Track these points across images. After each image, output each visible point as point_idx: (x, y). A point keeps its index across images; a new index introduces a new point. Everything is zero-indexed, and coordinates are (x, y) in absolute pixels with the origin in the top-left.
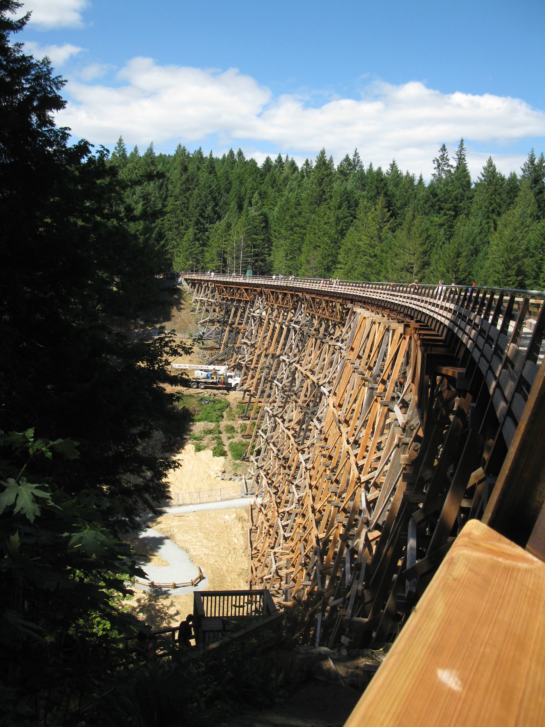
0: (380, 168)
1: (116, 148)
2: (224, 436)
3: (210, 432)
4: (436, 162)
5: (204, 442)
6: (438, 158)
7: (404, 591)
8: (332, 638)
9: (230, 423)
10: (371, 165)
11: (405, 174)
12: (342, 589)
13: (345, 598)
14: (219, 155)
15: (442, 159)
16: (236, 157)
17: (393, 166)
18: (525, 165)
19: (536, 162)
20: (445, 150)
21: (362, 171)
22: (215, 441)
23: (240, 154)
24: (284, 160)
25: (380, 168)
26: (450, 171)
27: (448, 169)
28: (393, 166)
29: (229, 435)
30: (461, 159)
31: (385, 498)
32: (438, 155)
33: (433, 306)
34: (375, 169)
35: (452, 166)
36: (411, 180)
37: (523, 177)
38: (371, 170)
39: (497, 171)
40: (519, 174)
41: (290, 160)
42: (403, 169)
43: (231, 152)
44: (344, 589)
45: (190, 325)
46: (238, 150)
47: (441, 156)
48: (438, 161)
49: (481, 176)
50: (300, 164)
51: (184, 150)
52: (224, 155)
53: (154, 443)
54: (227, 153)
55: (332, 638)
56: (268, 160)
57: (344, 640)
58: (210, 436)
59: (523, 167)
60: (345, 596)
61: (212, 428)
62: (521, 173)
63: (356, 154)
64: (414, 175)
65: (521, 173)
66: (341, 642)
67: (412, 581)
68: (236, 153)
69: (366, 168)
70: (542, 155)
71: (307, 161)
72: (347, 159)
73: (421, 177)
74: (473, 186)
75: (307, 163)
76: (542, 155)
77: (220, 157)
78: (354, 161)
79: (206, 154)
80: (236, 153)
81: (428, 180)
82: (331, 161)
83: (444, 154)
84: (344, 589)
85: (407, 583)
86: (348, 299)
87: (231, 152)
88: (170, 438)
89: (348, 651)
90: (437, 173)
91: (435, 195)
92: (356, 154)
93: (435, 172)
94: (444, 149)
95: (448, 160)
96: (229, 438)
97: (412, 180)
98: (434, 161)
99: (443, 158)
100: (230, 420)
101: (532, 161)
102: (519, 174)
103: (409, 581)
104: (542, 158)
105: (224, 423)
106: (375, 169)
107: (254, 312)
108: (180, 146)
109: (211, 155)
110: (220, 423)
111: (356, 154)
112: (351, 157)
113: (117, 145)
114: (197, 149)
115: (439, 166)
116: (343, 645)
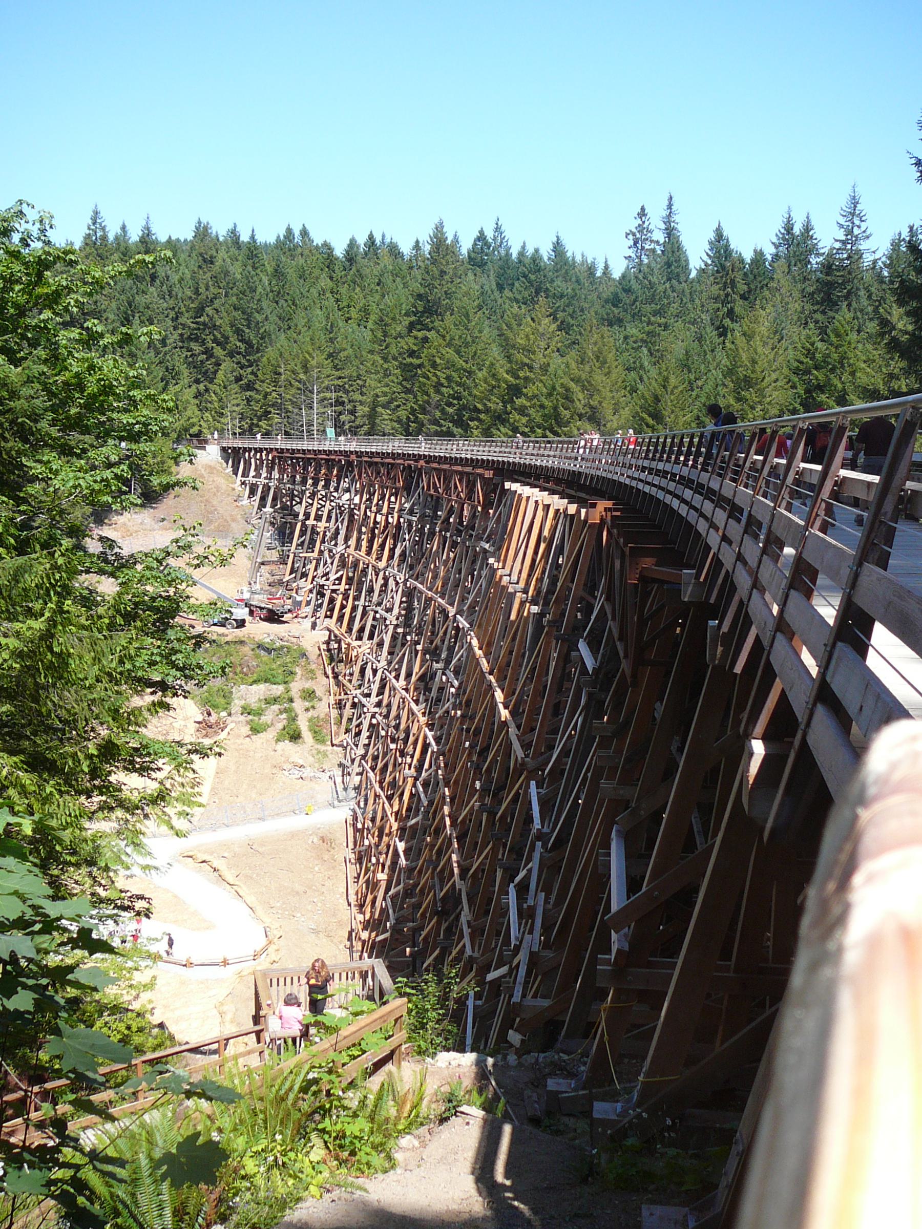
0: (537, 251)
1: (89, 229)
2: (299, 705)
3: (275, 700)
4: (631, 237)
5: (266, 718)
6: (634, 230)
7: (609, 951)
8: (493, 1035)
9: (308, 685)
10: (524, 247)
11: (578, 259)
12: (506, 951)
13: (511, 966)
14: (268, 235)
15: (640, 232)
16: (298, 238)
17: (558, 247)
18: (777, 235)
19: (797, 230)
20: (645, 215)
21: (508, 255)
22: (284, 716)
23: (304, 233)
24: (378, 242)
25: (537, 251)
26: (654, 250)
27: (652, 246)
28: (558, 247)
29: (307, 704)
30: (670, 232)
31: (570, 796)
32: (633, 224)
33: (650, 473)
34: (530, 251)
35: (657, 242)
36: (591, 270)
37: (776, 257)
38: (522, 254)
39: (732, 247)
40: (769, 251)
41: (388, 240)
42: (575, 250)
43: (289, 231)
44: (510, 950)
45: (233, 525)
46: (301, 227)
47: (639, 225)
48: (634, 235)
49: (706, 258)
50: (406, 248)
51: (206, 228)
52: (278, 237)
53: (183, 723)
54: (282, 233)
55: (493, 1035)
56: (352, 244)
57: (514, 1037)
58: (276, 707)
59: (775, 240)
60: (511, 963)
61: (279, 693)
62: (773, 250)
63: (498, 229)
64: (595, 259)
65: (773, 250)
66: (507, 1042)
67: (622, 932)
68: (297, 233)
69: (514, 253)
70: (808, 218)
71: (417, 242)
72: (481, 237)
73: (606, 267)
74: (693, 274)
75: (417, 246)
76: (808, 218)
77: (272, 240)
78: (495, 239)
79: (245, 238)
80: (297, 233)
81: (617, 273)
82: (456, 240)
83: (644, 222)
84: (510, 950)
85: (614, 936)
86: (568, 655)
87: (289, 231)
88: (209, 714)
89: (519, 1057)
90: (633, 255)
91: (628, 291)
92: (497, 228)
93: (631, 253)
94: (642, 213)
95: (651, 232)
96: (307, 710)
97: (591, 270)
98: (627, 234)
99: (641, 229)
100: (307, 679)
101: (789, 228)
102: (769, 251)
103: (616, 932)
104: (809, 222)
105: (296, 687)
106: (530, 251)
107: (339, 498)
108: (200, 223)
109: (253, 237)
110: (292, 685)
111: (498, 229)
112: (489, 234)
113: (90, 222)
114: (231, 227)
115: (636, 243)
116: (511, 1046)
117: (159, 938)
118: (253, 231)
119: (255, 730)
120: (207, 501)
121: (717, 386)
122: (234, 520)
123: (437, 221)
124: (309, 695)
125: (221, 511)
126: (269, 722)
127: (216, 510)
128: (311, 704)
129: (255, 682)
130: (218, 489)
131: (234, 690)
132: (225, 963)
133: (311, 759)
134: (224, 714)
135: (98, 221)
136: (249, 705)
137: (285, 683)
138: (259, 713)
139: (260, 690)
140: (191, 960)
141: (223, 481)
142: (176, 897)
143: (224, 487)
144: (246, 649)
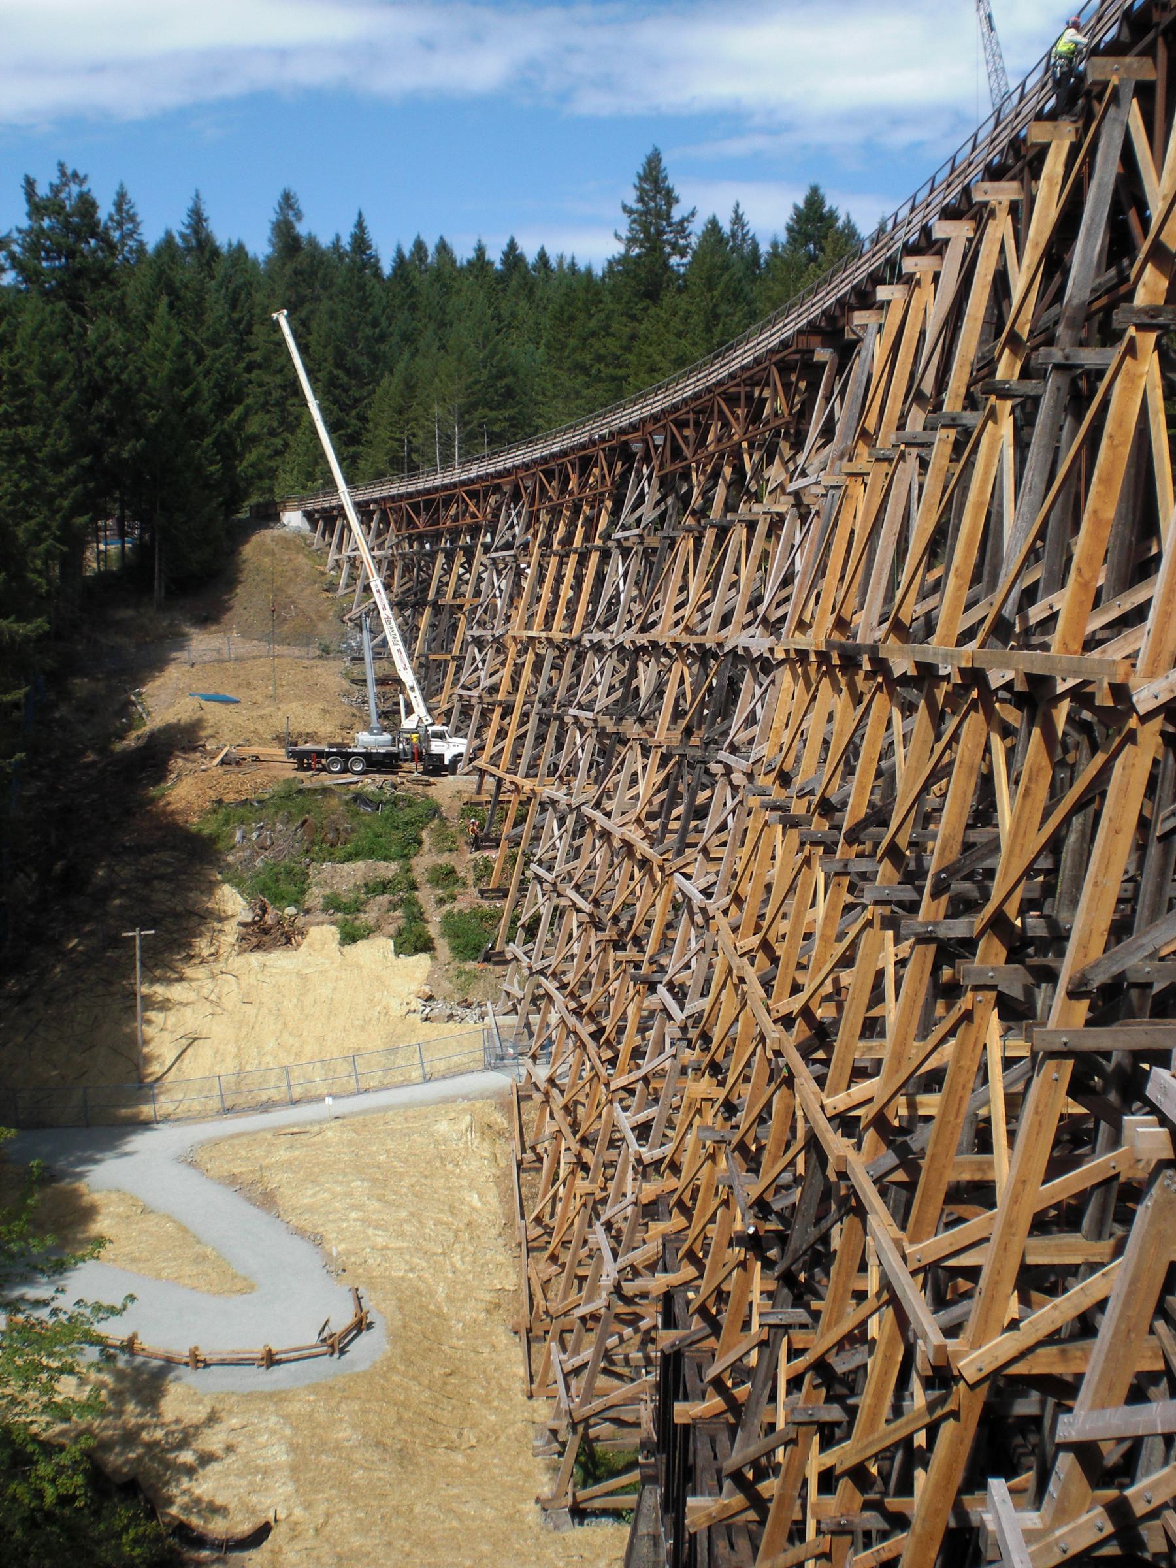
2: (426, 896)
3: (384, 886)
5: (368, 917)
9: (444, 859)
22: (399, 913)
29: (440, 892)
43: (419, 246)
45: (322, 626)
46: (436, 240)
58: (384, 899)
68: (431, 249)
80: (431, 249)
87: (419, 246)
96: (441, 901)
105: (424, 862)
110: (414, 861)
112: (726, 227)
117: (119, 1306)
118: (360, 215)
119: (350, 937)
120: (278, 589)
121: (538, 1539)
122: (323, 618)
123: (649, 151)
124: (446, 877)
125: (302, 604)
126: (372, 923)
127: (293, 602)
128: (448, 891)
129: (349, 858)
130: (296, 570)
131: (311, 871)
132: (271, 1360)
133: (447, 986)
134: (290, 910)
135: (125, 207)
136: (336, 896)
137: (404, 856)
138: (356, 907)
139: (356, 872)
140: (203, 1354)
141: (305, 560)
142: (184, 1230)
143: (307, 569)
144: (334, 802)
